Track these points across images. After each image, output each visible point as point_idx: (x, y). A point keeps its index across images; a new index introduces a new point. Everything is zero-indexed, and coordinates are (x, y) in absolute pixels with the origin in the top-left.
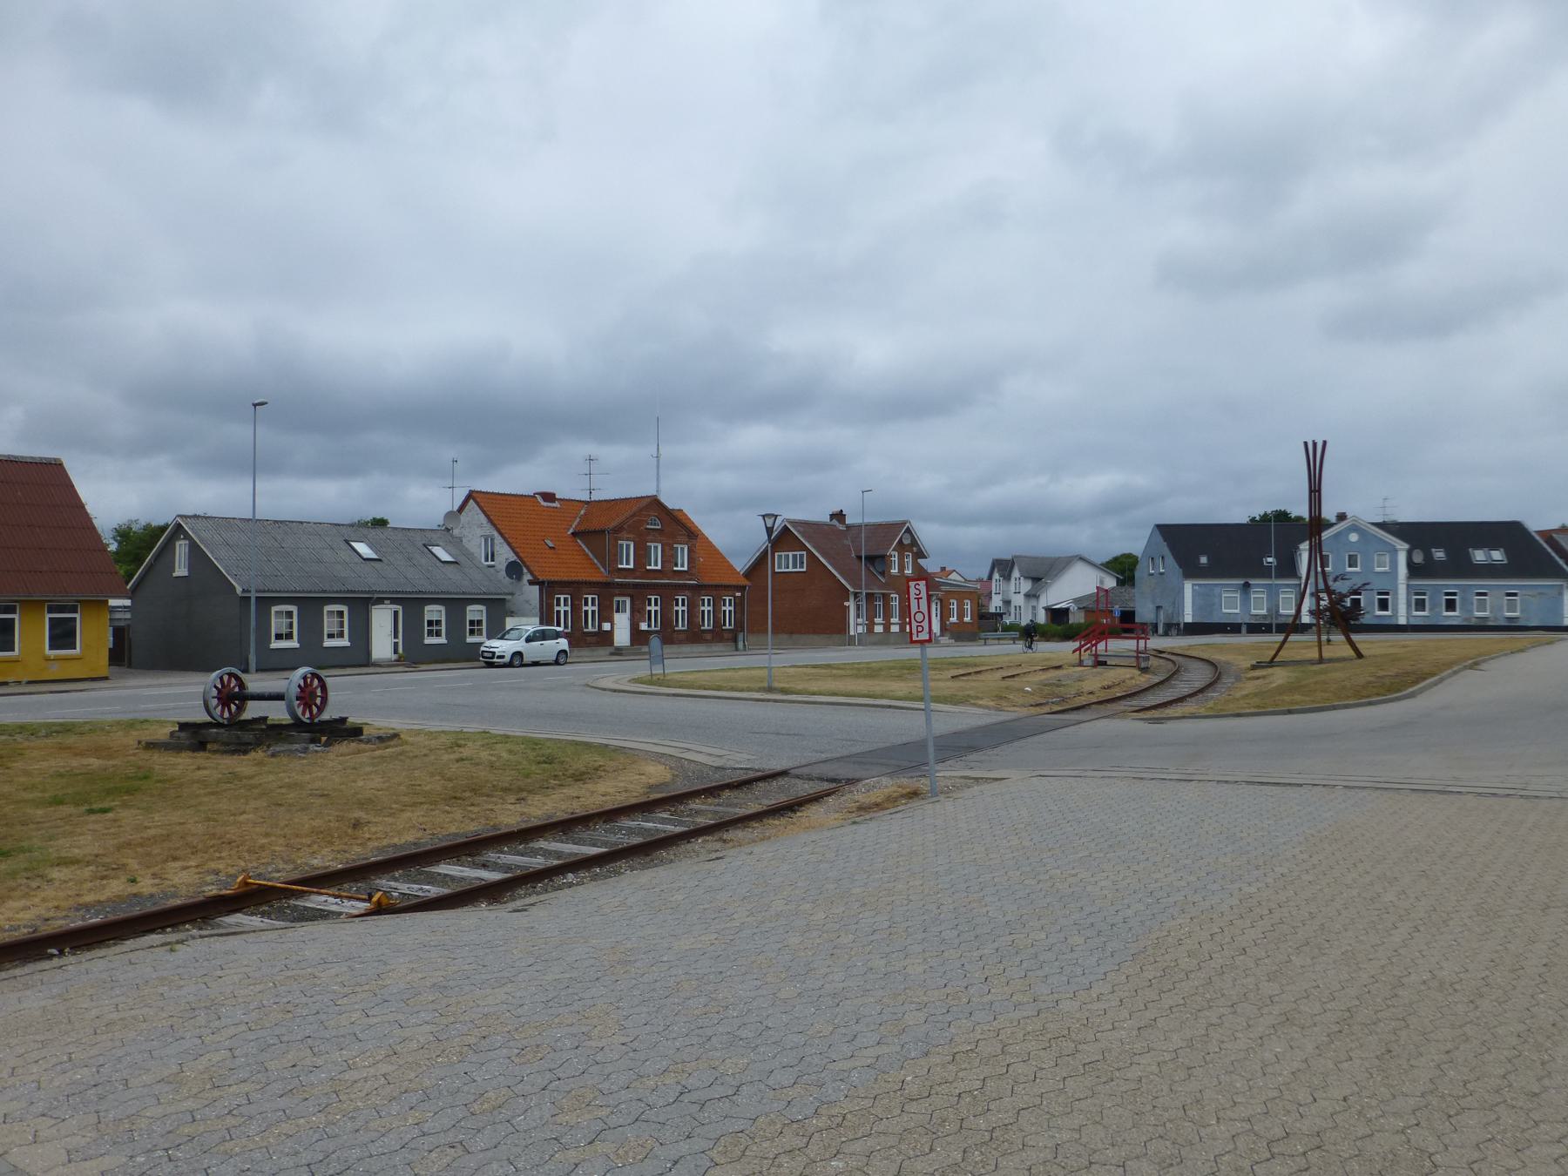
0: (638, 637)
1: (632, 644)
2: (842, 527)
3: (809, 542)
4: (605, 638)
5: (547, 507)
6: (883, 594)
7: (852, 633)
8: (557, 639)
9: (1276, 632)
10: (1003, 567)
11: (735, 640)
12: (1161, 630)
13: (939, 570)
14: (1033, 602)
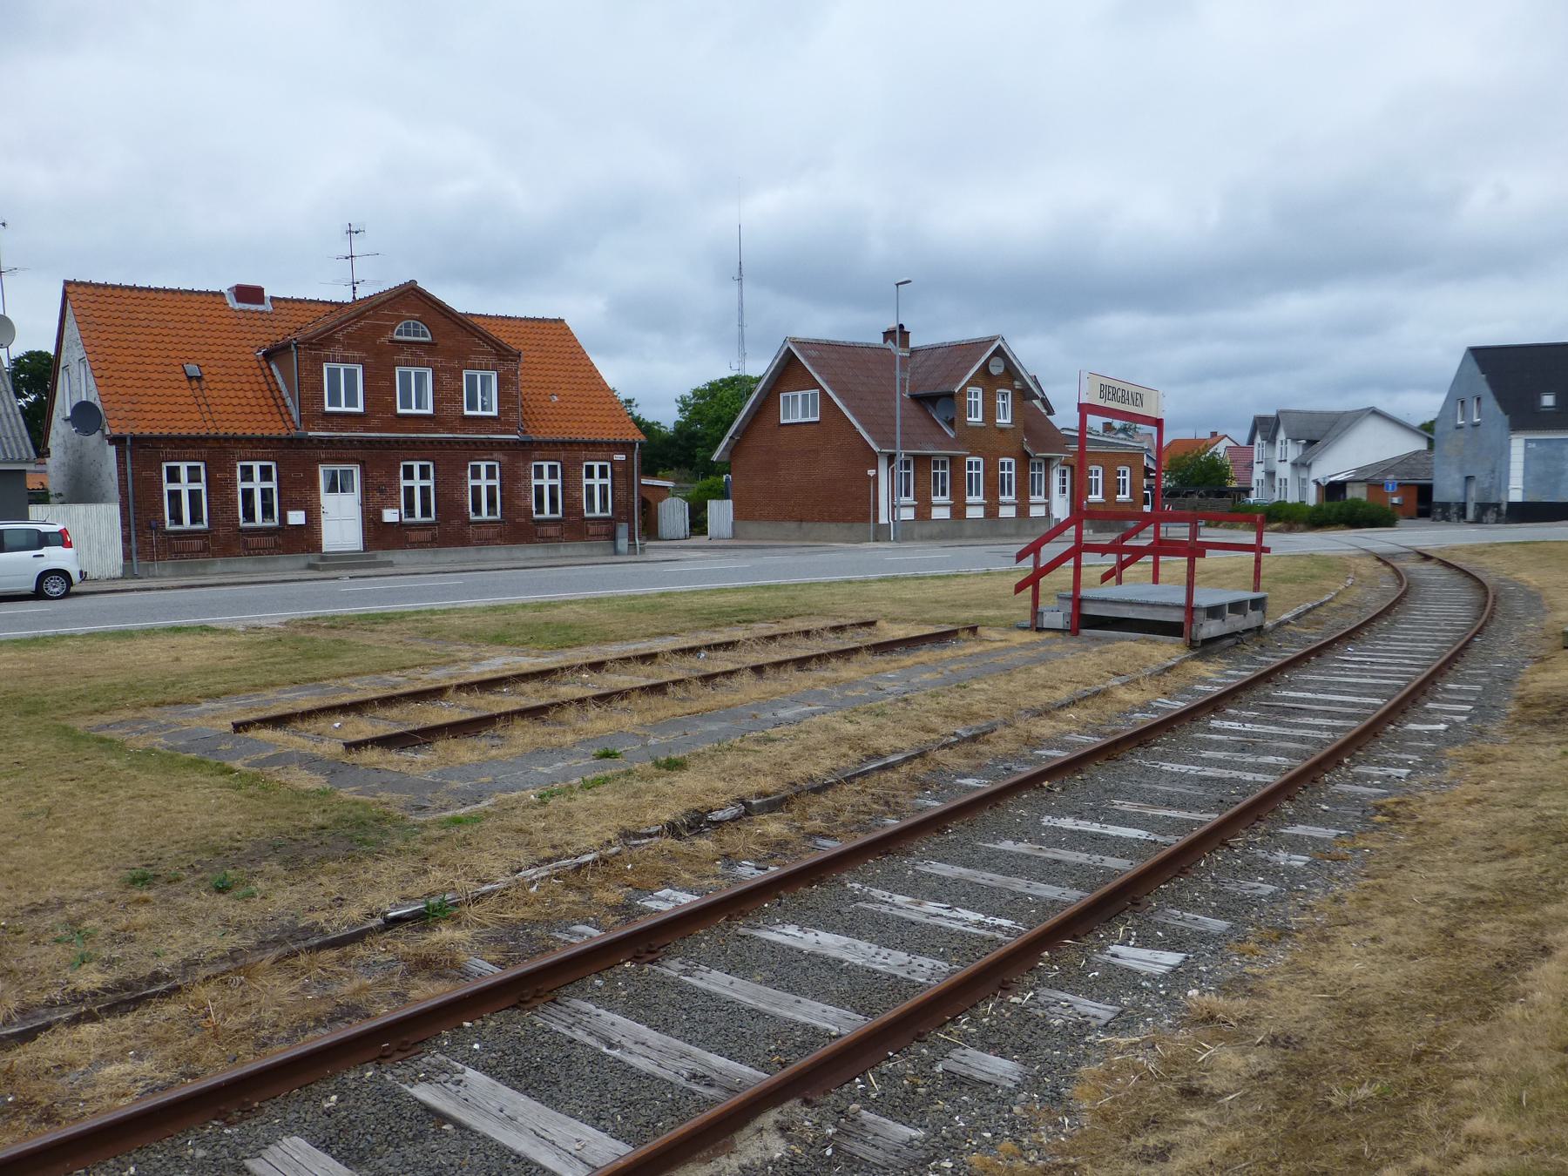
0: (377, 534)
1: (366, 548)
2: (900, 352)
3: (820, 374)
4: (305, 540)
5: (241, 310)
6: (952, 458)
7: (883, 520)
8: (40, 547)
9: (1225, 605)
10: (1266, 427)
11: (612, 536)
12: (1470, 514)
13: (1208, 436)
14: (1303, 475)
